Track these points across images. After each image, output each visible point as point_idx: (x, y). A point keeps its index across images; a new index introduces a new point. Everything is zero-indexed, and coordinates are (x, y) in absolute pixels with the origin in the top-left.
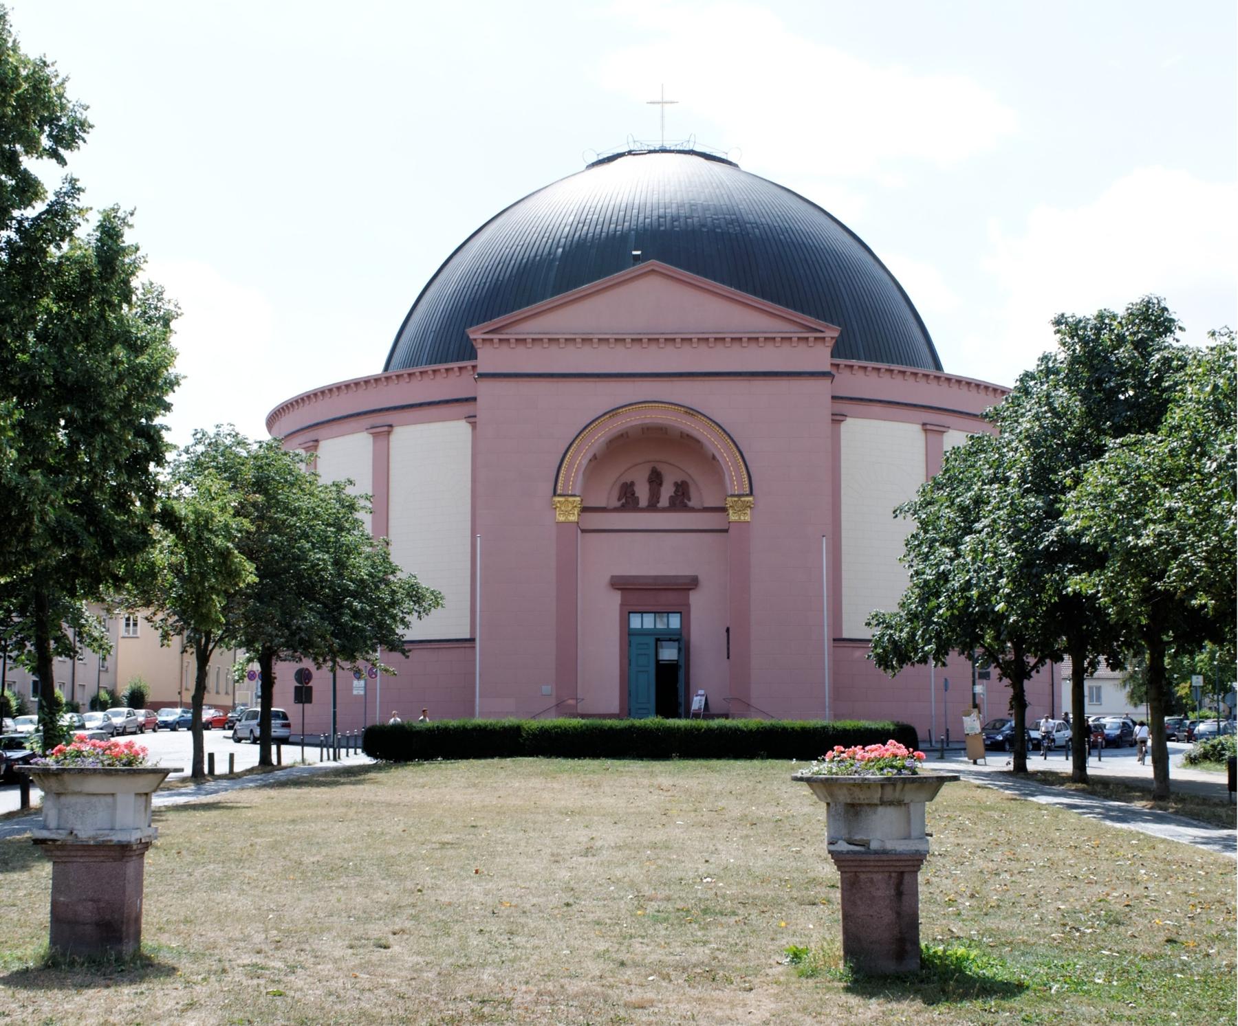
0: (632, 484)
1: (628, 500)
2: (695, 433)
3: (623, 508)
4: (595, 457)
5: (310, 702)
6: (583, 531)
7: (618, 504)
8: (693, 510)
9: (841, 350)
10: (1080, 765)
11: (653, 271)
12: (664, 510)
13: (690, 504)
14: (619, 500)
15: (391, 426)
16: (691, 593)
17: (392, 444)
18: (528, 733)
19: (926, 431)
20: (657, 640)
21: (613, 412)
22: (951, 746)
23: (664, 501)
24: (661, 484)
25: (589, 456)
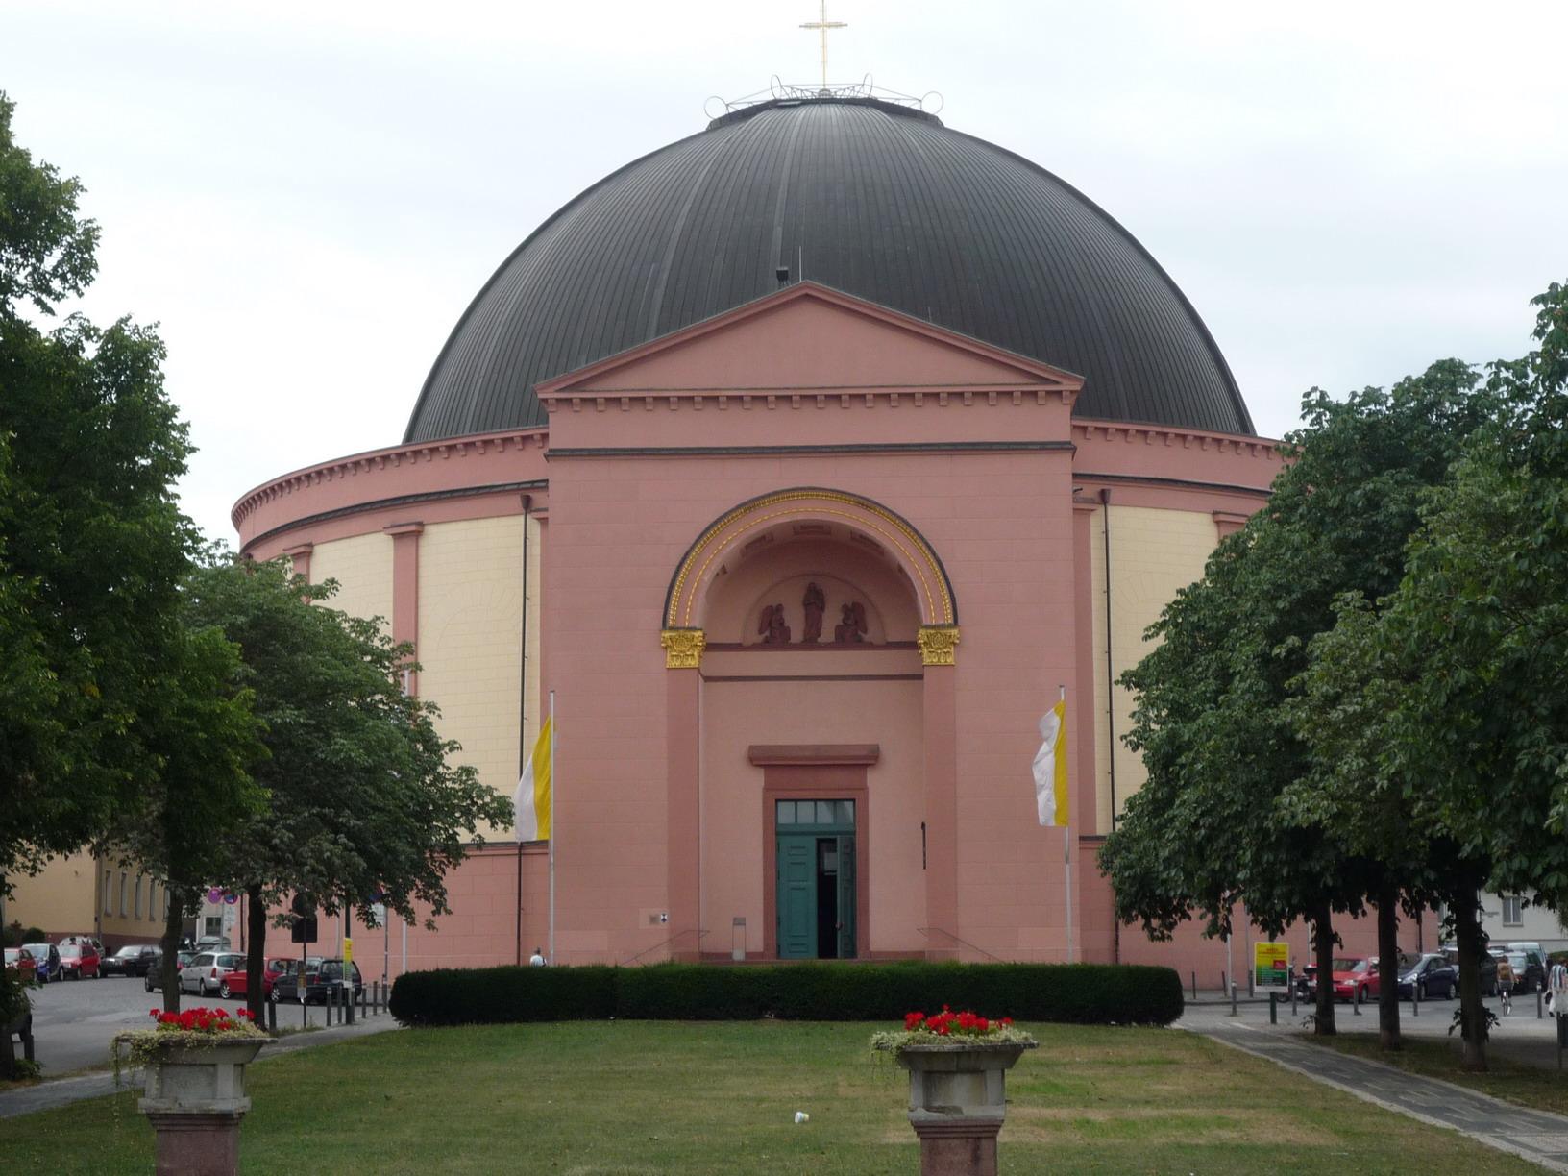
0: (780, 608)
1: (773, 633)
2: (872, 534)
3: (767, 645)
4: (724, 570)
5: (314, 940)
6: (707, 679)
7: (760, 639)
8: (871, 646)
9: (1082, 407)
10: (1390, 1019)
11: (807, 295)
12: (827, 647)
13: (867, 638)
14: (761, 632)
15: (421, 524)
16: (869, 771)
17: (423, 561)
18: (1160, 785)
19: (1218, 523)
20: (819, 841)
21: (750, 506)
22: (1200, 997)
23: (828, 634)
24: (822, 609)
25: (715, 568)
